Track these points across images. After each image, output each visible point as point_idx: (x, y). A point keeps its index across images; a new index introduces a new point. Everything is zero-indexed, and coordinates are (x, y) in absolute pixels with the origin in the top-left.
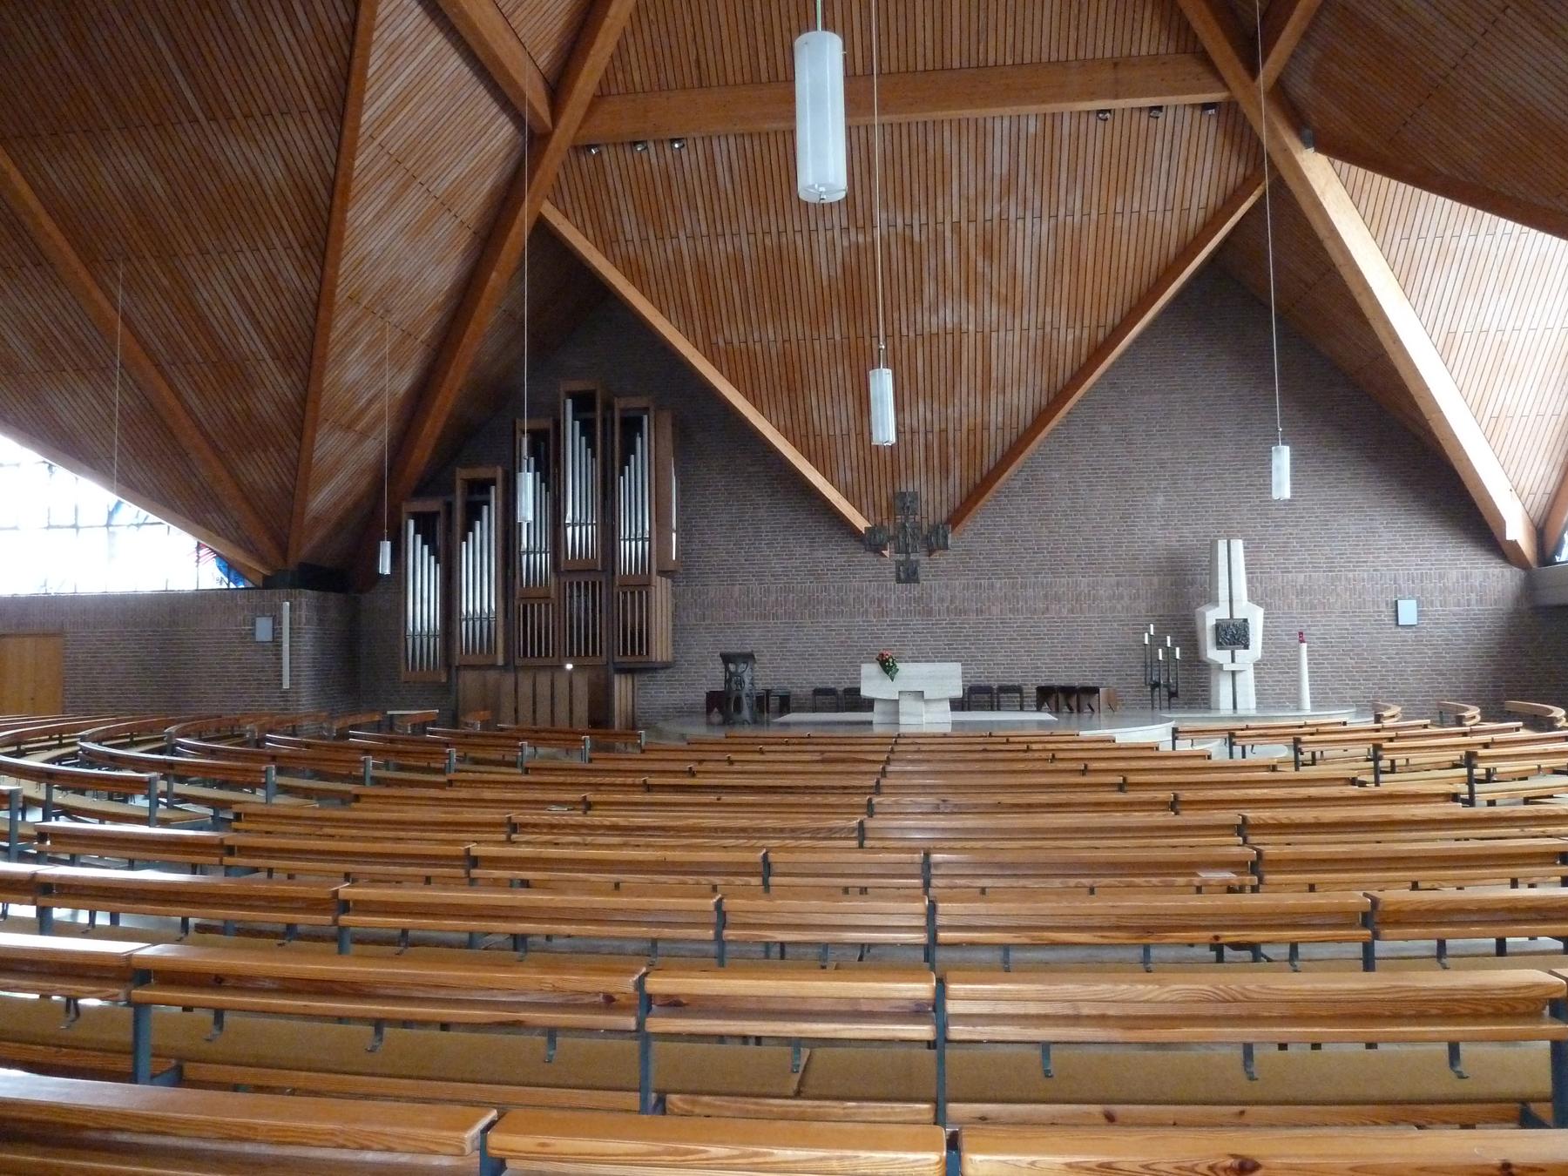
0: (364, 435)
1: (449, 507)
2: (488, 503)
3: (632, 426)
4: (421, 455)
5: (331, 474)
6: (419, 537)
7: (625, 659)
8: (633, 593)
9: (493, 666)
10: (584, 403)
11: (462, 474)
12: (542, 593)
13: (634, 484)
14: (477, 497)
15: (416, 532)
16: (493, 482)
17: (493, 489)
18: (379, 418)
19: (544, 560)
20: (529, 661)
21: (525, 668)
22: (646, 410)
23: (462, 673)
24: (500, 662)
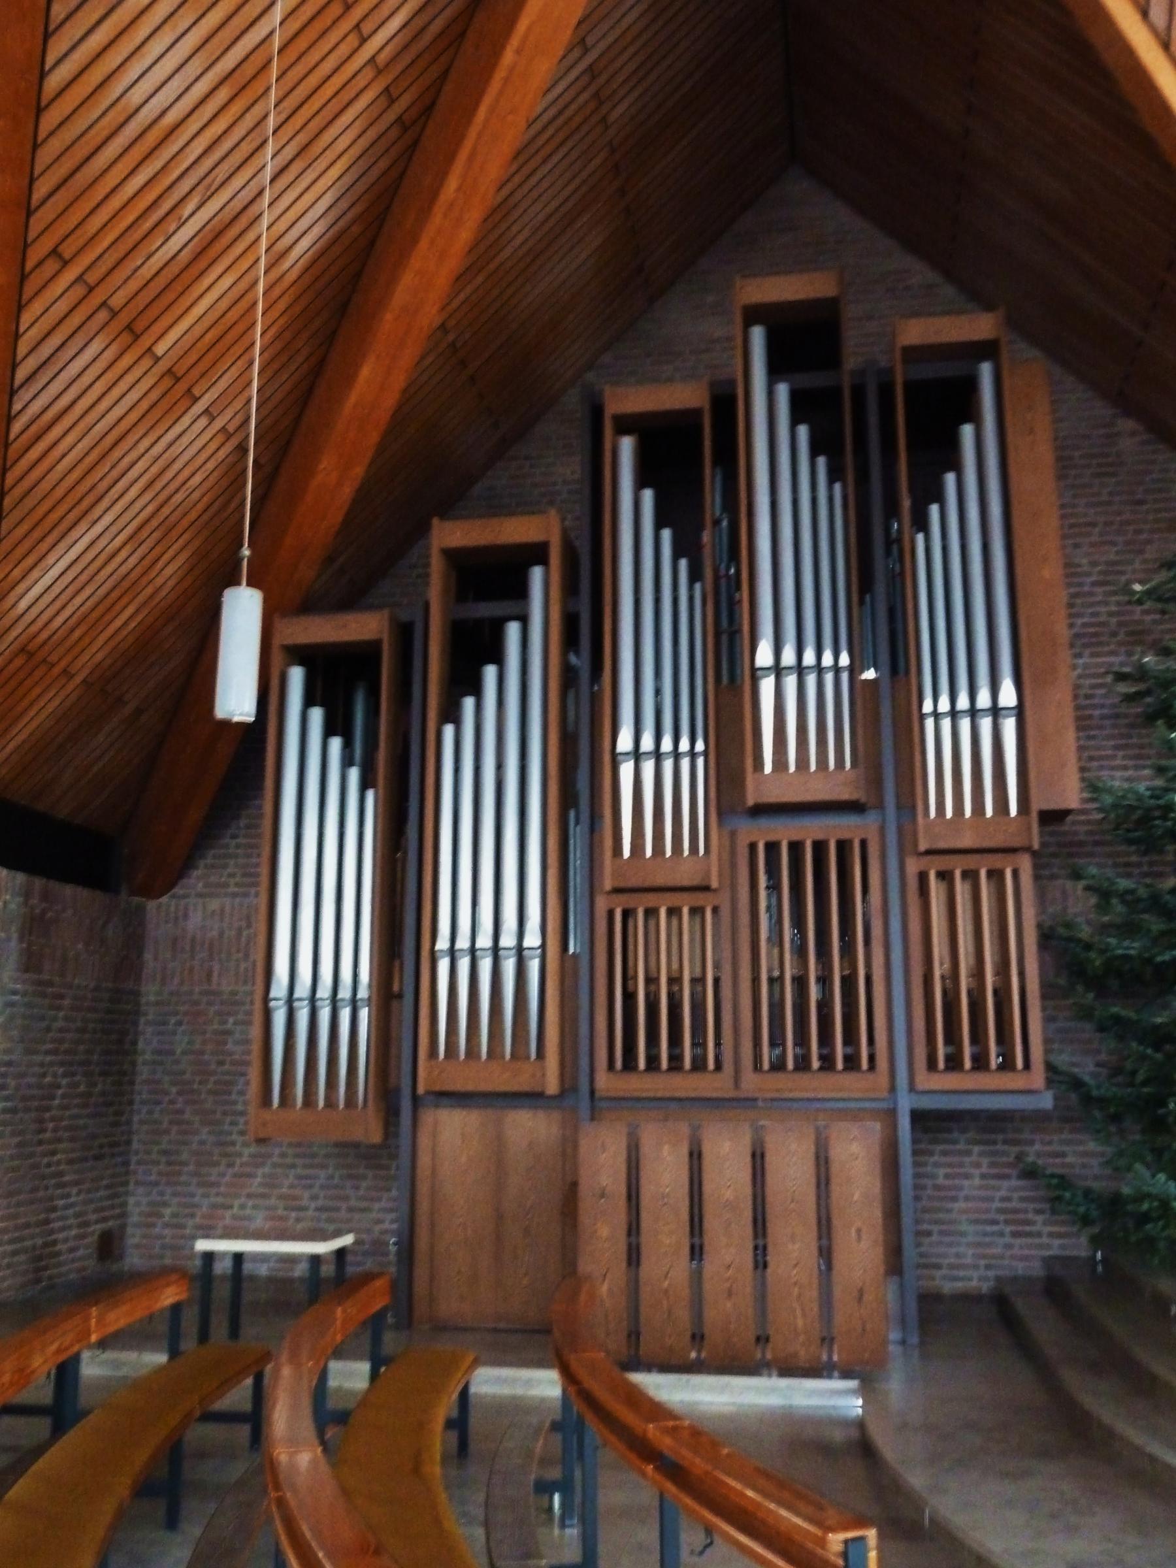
0: (178, 387)
1: (406, 635)
2: (524, 620)
3: (938, 407)
4: (335, 478)
5: (78, 505)
6: (317, 715)
7: (951, 1081)
8: (996, 875)
9: (532, 1098)
10: (803, 341)
11: (451, 534)
12: (685, 875)
13: (955, 549)
14: (486, 610)
15: (309, 701)
16: (538, 553)
17: (537, 574)
18: (226, 337)
19: (690, 780)
20: (640, 1084)
21: (780, 1105)
22: (987, 350)
23: (428, 1117)
24: (552, 1086)
